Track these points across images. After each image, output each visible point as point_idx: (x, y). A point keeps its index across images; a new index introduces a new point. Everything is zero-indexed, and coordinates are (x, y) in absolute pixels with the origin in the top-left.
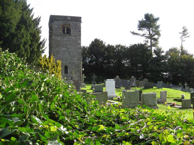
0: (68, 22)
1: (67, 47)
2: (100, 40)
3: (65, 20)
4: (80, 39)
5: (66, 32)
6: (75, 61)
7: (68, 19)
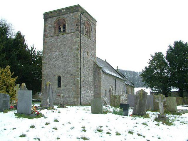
0: (63, 16)
1: (61, 50)
2: (173, 46)
3: (58, 15)
4: (95, 49)
5: (62, 30)
6: (70, 69)
7: (63, 12)
